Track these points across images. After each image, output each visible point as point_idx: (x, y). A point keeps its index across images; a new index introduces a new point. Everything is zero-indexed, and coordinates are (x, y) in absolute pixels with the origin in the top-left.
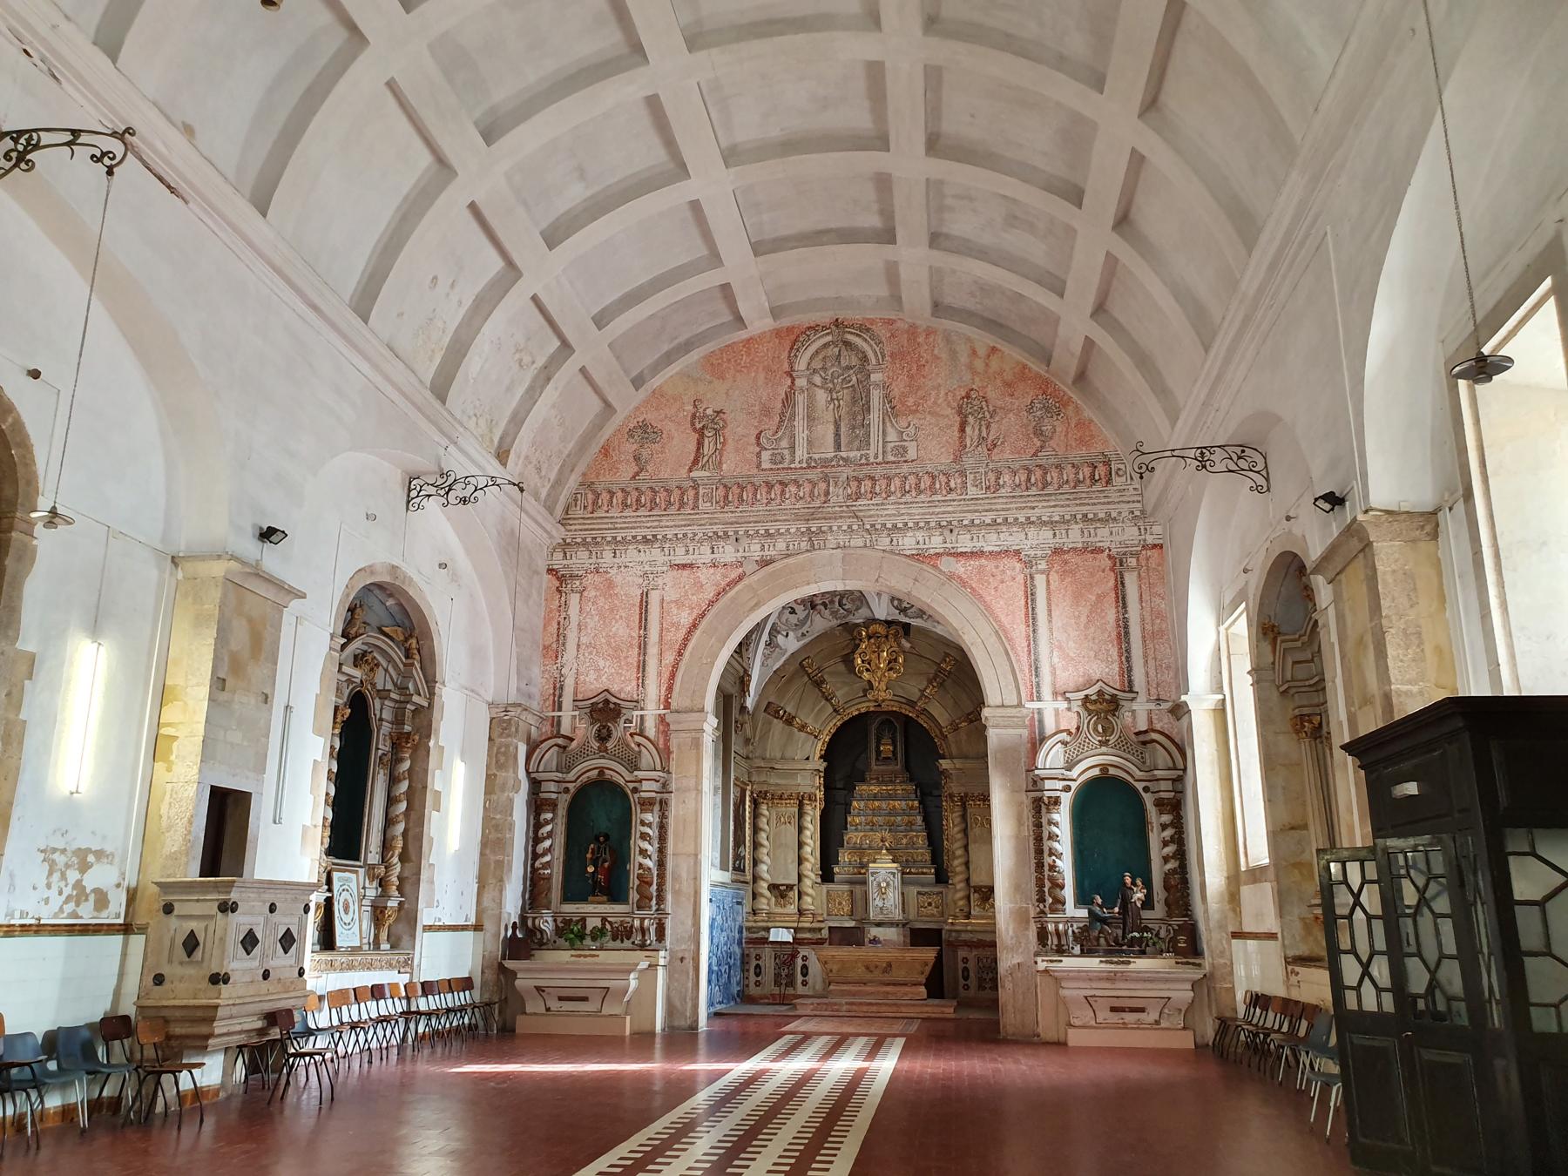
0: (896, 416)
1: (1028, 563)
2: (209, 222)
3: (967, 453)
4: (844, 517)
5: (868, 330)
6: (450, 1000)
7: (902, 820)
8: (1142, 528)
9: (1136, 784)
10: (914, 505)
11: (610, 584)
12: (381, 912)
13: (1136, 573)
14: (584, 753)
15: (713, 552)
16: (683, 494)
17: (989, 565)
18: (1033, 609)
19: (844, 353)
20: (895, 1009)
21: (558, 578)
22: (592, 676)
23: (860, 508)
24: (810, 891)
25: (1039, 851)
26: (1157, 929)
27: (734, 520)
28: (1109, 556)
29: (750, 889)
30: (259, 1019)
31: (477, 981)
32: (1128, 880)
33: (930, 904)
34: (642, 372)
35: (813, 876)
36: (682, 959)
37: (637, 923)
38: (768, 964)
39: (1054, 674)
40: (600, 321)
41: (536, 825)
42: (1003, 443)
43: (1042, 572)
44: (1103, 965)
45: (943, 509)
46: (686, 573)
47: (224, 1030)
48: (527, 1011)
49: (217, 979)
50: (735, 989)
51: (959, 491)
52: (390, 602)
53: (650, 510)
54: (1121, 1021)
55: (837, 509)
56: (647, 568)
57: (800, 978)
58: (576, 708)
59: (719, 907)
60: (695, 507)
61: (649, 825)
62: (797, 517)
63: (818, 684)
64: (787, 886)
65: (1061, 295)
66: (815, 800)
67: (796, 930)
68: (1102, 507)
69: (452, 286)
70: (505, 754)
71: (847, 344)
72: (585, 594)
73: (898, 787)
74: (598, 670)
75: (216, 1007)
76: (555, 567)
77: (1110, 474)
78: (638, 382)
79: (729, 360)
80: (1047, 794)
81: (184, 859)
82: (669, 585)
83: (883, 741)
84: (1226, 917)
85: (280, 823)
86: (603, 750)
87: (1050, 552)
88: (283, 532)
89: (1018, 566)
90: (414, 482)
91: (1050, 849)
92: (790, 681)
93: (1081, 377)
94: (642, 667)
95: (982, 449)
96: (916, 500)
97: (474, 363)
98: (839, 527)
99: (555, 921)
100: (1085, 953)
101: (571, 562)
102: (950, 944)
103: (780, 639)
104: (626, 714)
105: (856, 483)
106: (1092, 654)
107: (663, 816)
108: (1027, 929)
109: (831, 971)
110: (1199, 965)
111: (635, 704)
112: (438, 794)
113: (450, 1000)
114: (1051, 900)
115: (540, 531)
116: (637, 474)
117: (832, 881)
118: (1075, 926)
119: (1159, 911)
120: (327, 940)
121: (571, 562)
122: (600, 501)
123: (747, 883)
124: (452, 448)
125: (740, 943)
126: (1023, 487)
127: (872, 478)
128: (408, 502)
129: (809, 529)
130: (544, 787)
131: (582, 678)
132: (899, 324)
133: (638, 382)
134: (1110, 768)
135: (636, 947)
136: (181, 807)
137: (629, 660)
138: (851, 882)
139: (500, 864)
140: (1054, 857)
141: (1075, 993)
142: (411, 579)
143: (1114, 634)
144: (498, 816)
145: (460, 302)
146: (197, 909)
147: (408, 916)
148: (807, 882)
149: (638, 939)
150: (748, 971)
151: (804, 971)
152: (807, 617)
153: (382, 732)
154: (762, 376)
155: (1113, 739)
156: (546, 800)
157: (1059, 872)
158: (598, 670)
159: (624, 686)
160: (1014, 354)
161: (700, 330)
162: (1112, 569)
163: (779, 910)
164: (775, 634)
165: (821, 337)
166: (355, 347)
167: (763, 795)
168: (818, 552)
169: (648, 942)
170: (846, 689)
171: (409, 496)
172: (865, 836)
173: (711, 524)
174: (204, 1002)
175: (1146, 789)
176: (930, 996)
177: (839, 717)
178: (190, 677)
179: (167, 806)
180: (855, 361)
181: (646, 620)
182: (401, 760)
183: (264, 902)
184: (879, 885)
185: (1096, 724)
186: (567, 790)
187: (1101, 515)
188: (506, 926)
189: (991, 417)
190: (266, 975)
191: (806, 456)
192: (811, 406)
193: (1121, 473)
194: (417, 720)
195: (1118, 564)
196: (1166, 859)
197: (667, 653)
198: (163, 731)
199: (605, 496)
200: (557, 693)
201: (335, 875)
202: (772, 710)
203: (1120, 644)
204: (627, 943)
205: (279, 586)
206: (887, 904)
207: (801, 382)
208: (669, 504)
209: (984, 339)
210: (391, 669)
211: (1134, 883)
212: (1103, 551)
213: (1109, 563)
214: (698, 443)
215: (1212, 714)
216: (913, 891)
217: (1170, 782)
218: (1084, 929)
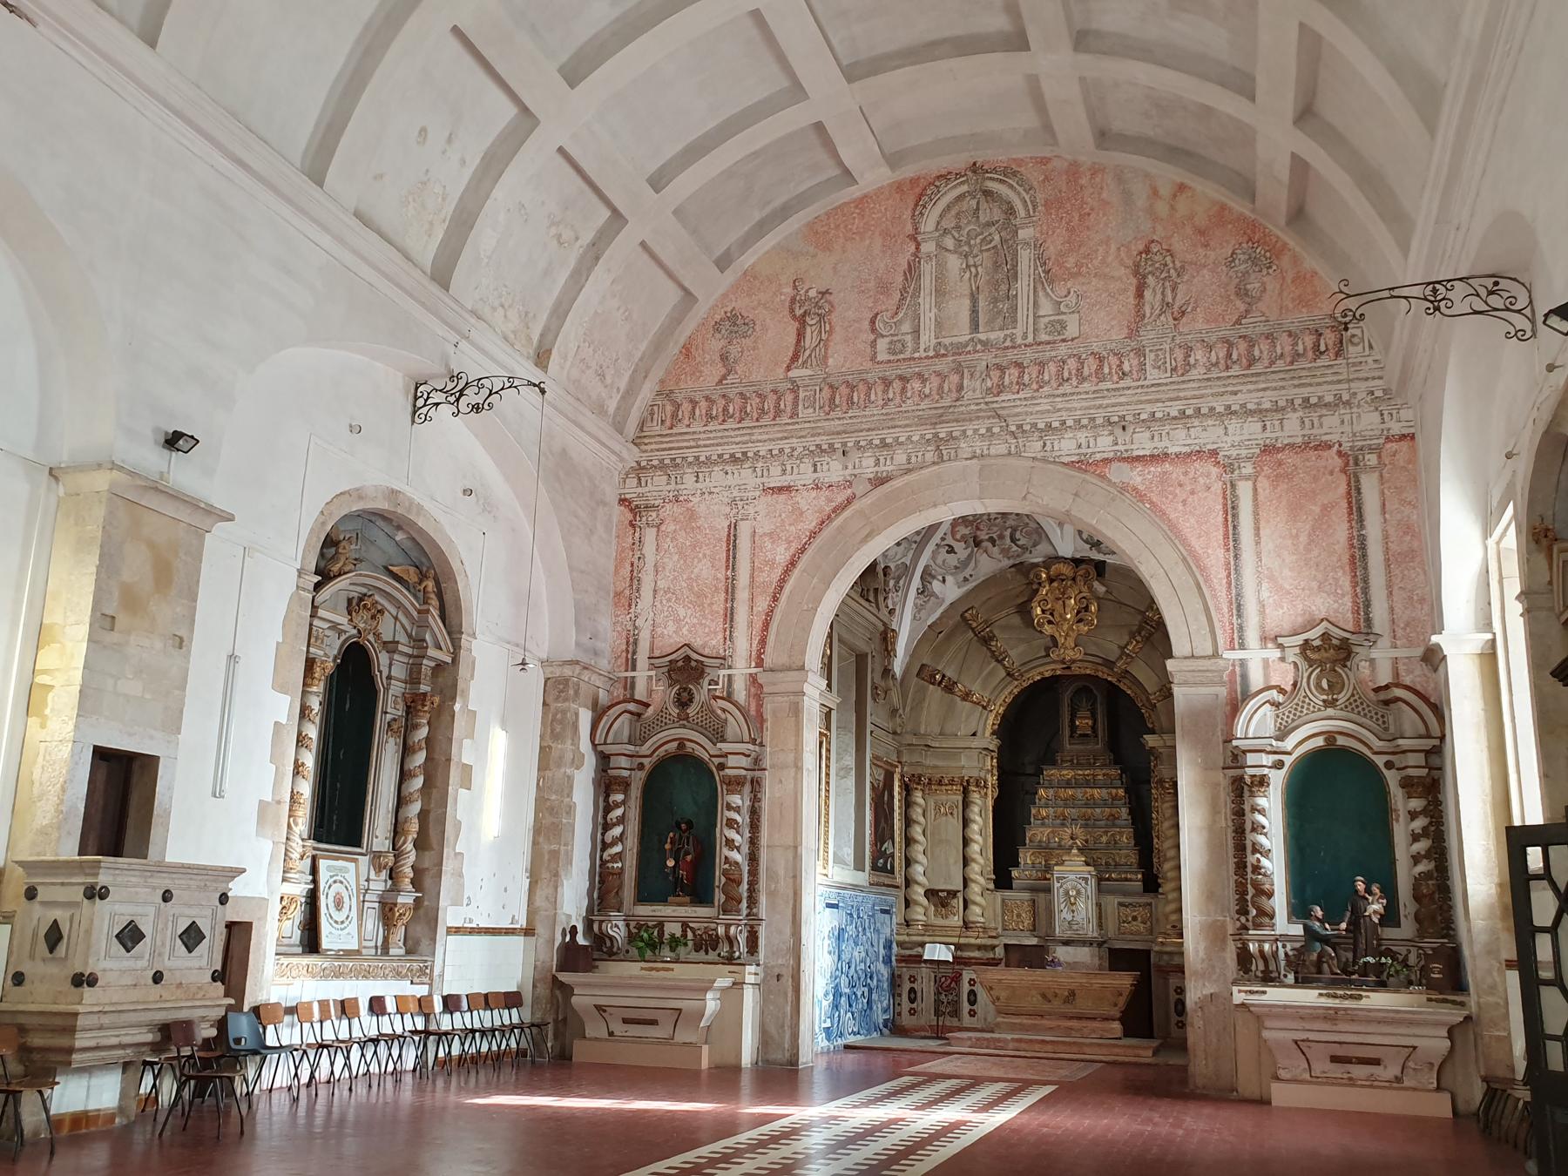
0: (1051, 282)
1: (1229, 467)
2: (73, 53)
3: (1145, 325)
4: (983, 417)
5: (1015, 174)
6: (486, 1018)
7: (1102, 812)
8: (1386, 413)
9: (1374, 758)
10: (1074, 397)
11: (692, 515)
12: (391, 909)
13: (1377, 474)
14: (661, 721)
15: (815, 471)
16: (779, 399)
17: (1175, 471)
18: (1235, 527)
19: (983, 205)
20: (1075, 1049)
21: (631, 510)
22: (671, 627)
23: (1004, 405)
24: (978, 899)
25: (1240, 848)
26: (1404, 953)
27: (842, 428)
28: (1339, 453)
29: (901, 894)
30: (149, 1032)
31: (527, 997)
32: (1361, 886)
33: (1135, 918)
34: (729, 249)
35: (982, 880)
36: (779, 977)
37: (721, 930)
38: (926, 987)
39: (1262, 612)
40: (657, 182)
41: (604, 807)
42: (1194, 309)
43: (1247, 478)
44: (1323, 1000)
45: (1113, 401)
46: (782, 497)
47: (92, 1043)
48: (587, 1036)
49: (82, 980)
50: (880, 1017)
51: (1135, 376)
52: (400, 536)
53: (740, 422)
54: (1346, 1076)
55: (973, 407)
56: (736, 493)
57: (966, 1007)
58: (653, 667)
59: (851, 915)
60: (794, 414)
61: (738, 810)
62: (922, 421)
63: (986, 641)
64: (949, 892)
65: (1252, 98)
66: (985, 787)
67: (958, 947)
68: (1330, 387)
69: (449, 140)
70: (561, 722)
71: (987, 193)
72: (663, 528)
73: (1098, 771)
74: (678, 621)
75: (76, 1014)
76: (628, 496)
77: (1341, 342)
78: (723, 263)
79: (837, 227)
80: (1250, 771)
81: (55, 835)
82: (762, 513)
83: (1079, 714)
84: (1498, 939)
85: (223, 797)
86: (684, 717)
87: (1258, 451)
88: (192, 437)
89: (1215, 471)
90: (420, 390)
91: (1254, 844)
92: (950, 636)
93: (1298, 215)
94: (730, 616)
95: (1167, 319)
96: (1077, 390)
97: (485, 237)
98: (976, 431)
99: (628, 925)
100: (1302, 982)
101: (647, 489)
102: (1160, 969)
103: (936, 586)
104: (711, 674)
105: (998, 373)
106: (1315, 584)
107: (755, 799)
108: (1224, 950)
109: (998, 999)
110: (1462, 1004)
111: (720, 661)
112: (467, 769)
113: (486, 1018)
114: (1254, 912)
115: (606, 452)
116: (724, 377)
117: (1010, 887)
118: (1289, 946)
119: (1407, 928)
120: (311, 941)
121: (647, 489)
122: (680, 413)
123: (897, 887)
124: (463, 345)
125: (887, 961)
126: (1222, 365)
127: (1019, 365)
128: (415, 412)
129: (936, 435)
130: (614, 762)
131: (659, 630)
132: (1056, 163)
133: (723, 263)
134: (1337, 737)
135: (722, 961)
136: (54, 770)
137: (715, 607)
138: (1033, 890)
139: (555, 855)
140: (1258, 855)
141: (1280, 1035)
142: (420, 508)
143: (1346, 558)
144: (554, 797)
145: (463, 162)
146: (61, 894)
147: (426, 915)
148: (975, 889)
149: (724, 949)
150: (900, 995)
151: (972, 998)
152: (970, 557)
153: (391, 692)
154: (878, 241)
155: (1342, 698)
156: (616, 778)
157: (1265, 875)
158: (678, 621)
159: (707, 639)
160: (1208, 190)
161: (801, 190)
162: (1344, 471)
163: (940, 922)
164: (929, 579)
165: (955, 187)
166: (303, 211)
167: (916, 778)
168: (947, 464)
169: (737, 954)
170: (1022, 648)
171: (415, 406)
172: (1052, 832)
173: (812, 436)
174: (61, 1008)
175: (1389, 765)
176: (1128, 1033)
177: (1016, 683)
178: (69, 613)
179: (40, 771)
180: (997, 214)
181: (734, 558)
182: (416, 727)
183: (154, 888)
184: (1067, 893)
185: (1319, 679)
186: (641, 767)
187: (1329, 398)
188: (564, 930)
189: (1178, 275)
190: (158, 978)
191: (934, 341)
192: (940, 279)
193: (1355, 340)
194: (440, 679)
195: (1351, 462)
196: (1416, 859)
197: (760, 598)
198: (39, 679)
199: (686, 407)
200: (630, 649)
201: (323, 864)
202: (926, 674)
203: (1354, 570)
204: (712, 956)
205: (193, 504)
206: (1078, 918)
207: (928, 247)
208: (763, 412)
209: (1168, 174)
210: (401, 617)
211: (1368, 891)
212: (1330, 447)
213: (1339, 462)
214: (799, 335)
215: (1477, 661)
216: (1112, 902)
217: (1423, 755)
218: (1300, 952)
